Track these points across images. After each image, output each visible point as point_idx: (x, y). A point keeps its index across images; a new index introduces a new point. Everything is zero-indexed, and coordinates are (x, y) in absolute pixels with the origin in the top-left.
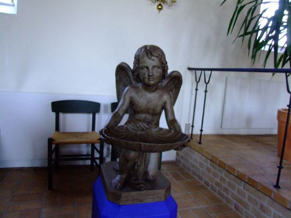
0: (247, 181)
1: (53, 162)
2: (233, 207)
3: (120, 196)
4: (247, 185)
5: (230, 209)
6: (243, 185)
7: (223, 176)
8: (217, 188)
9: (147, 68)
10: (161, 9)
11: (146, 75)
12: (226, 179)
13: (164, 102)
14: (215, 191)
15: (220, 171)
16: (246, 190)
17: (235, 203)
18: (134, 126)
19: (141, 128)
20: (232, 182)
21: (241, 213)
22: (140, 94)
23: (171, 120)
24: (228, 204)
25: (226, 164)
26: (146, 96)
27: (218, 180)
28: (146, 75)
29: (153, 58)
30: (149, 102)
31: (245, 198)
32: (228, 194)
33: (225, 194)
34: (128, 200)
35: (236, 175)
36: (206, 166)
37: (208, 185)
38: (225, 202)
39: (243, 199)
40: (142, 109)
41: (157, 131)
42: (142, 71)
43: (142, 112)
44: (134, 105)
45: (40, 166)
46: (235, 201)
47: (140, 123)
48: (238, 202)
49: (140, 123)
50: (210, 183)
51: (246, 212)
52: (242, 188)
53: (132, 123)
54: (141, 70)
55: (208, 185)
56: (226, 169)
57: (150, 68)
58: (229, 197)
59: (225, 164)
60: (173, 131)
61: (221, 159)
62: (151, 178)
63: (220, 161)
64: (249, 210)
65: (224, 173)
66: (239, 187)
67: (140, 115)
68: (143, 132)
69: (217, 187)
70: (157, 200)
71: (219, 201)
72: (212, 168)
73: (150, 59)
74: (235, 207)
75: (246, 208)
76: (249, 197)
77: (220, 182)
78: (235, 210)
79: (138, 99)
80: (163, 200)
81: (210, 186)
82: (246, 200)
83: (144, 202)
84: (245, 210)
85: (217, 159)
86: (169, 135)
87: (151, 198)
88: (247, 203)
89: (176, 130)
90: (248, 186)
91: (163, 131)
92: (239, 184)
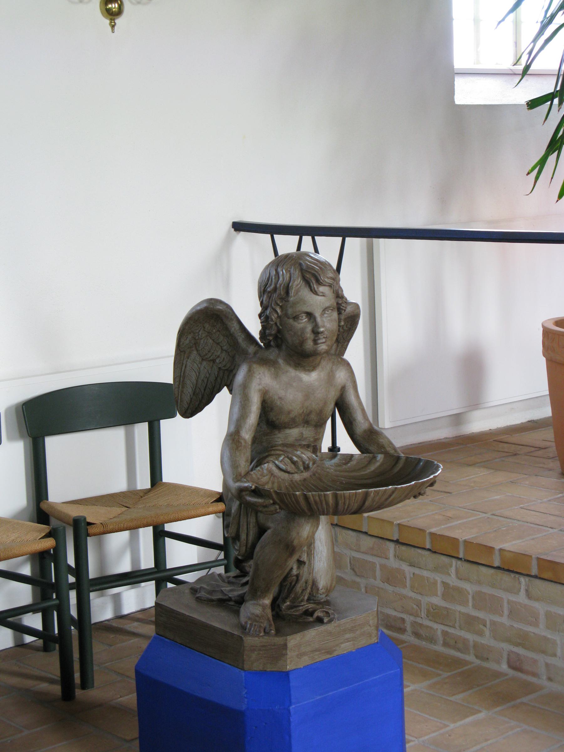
0: (534, 571)
1: (54, 597)
2: (504, 667)
3: (285, 646)
4: (538, 582)
5: (498, 675)
6: (523, 588)
7: (453, 580)
8: (439, 628)
9: (310, 315)
10: (119, 12)
11: (309, 335)
12: (466, 586)
13: (340, 387)
14: (432, 640)
15: (436, 569)
16: (537, 599)
17: (510, 653)
18: (285, 464)
19: (304, 463)
20: (487, 590)
21: (534, 675)
22: (284, 378)
23: (365, 431)
24: (485, 664)
25: (457, 540)
26: (300, 380)
27: (437, 601)
28: (309, 335)
29: (322, 289)
30: (307, 396)
31: (536, 624)
32: (480, 633)
33: (470, 637)
34: (304, 654)
35: (496, 564)
36: (383, 567)
37: (402, 630)
38: (478, 662)
39: (530, 629)
40: (292, 415)
41: (338, 465)
42: (295, 324)
43: (292, 424)
44: (272, 409)
45: (108, 590)
46: (506, 647)
47: (299, 453)
48: (518, 645)
49: (299, 453)
50: (409, 619)
51: (547, 665)
52: (522, 598)
53: (280, 455)
54: (291, 321)
55: (402, 630)
56: (461, 556)
57: (317, 315)
58: (487, 640)
59: (454, 541)
60: (380, 457)
61: (433, 530)
62: (322, 597)
63: (432, 534)
64: (555, 655)
65: (453, 570)
66: (513, 598)
67: (288, 431)
68: (306, 475)
69: (435, 626)
70: (363, 642)
71: (456, 663)
72: (405, 567)
73: (316, 293)
74: (510, 666)
75: (544, 652)
76: (548, 615)
77: (443, 604)
78: (511, 672)
79: (282, 393)
80: (374, 640)
81: (409, 628)
82: (541, 630)
83: (335, 654)
84: (541, 659)
85: (422, 531)
86: (372, 468)
87: (348, 640)
88: (546, 639)
89: (386, 454)
90: (540, 586)
91: (353, 463)
92: (508, 590)
